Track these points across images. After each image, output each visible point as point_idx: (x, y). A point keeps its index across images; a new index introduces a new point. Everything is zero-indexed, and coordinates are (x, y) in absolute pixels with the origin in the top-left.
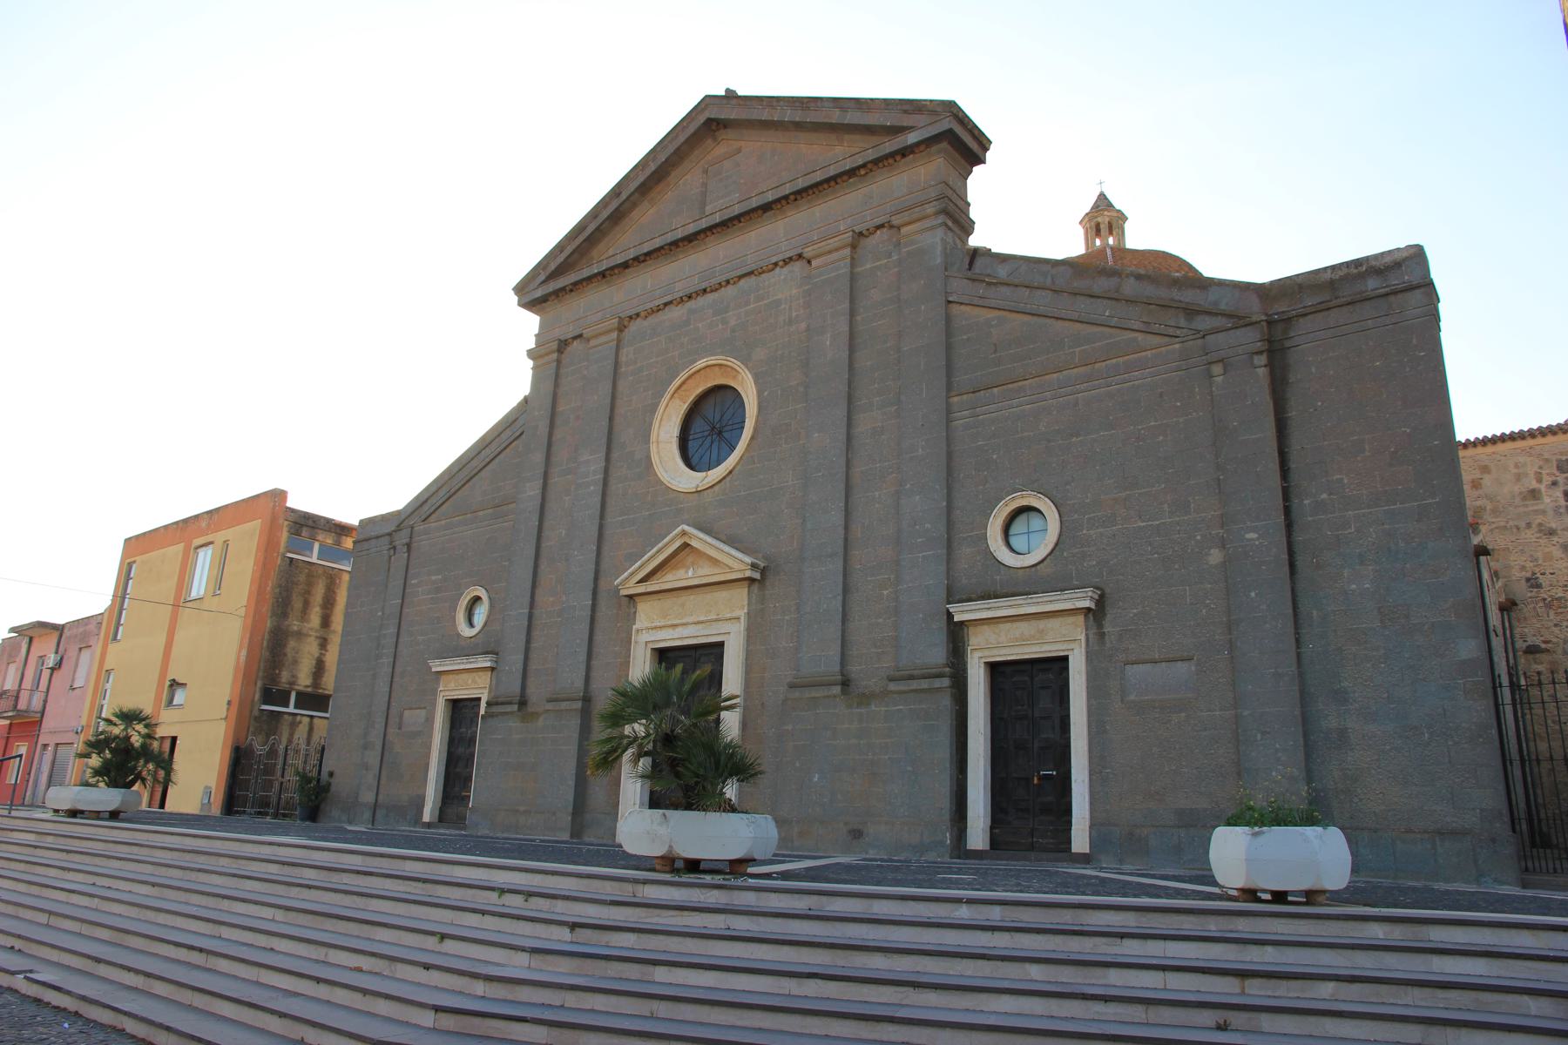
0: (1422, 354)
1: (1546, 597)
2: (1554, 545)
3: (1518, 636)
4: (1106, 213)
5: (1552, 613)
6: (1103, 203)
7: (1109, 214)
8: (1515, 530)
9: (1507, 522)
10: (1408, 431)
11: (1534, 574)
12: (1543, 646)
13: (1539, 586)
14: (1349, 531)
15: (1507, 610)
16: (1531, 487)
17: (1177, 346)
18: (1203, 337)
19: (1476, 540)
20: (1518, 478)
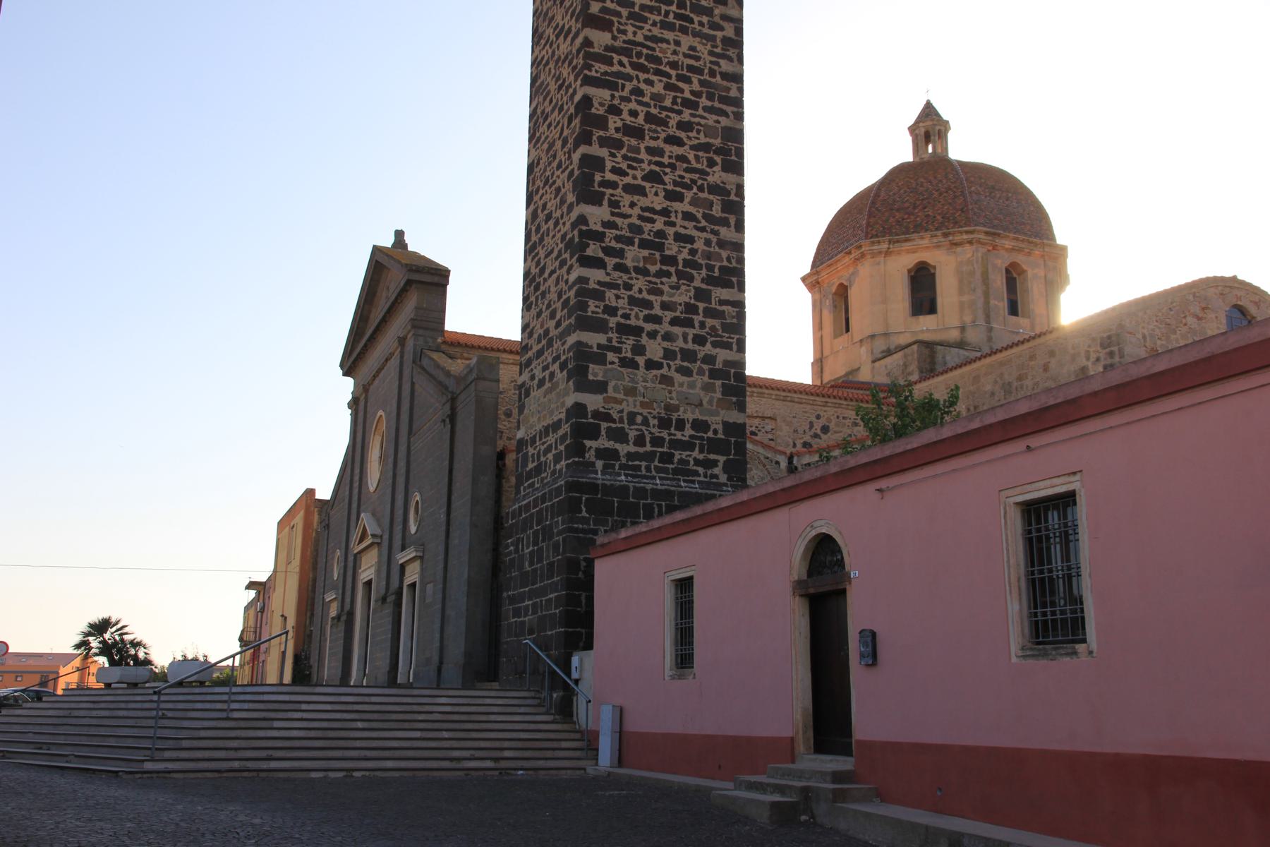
6: (929, 112)
7: (924, 124)
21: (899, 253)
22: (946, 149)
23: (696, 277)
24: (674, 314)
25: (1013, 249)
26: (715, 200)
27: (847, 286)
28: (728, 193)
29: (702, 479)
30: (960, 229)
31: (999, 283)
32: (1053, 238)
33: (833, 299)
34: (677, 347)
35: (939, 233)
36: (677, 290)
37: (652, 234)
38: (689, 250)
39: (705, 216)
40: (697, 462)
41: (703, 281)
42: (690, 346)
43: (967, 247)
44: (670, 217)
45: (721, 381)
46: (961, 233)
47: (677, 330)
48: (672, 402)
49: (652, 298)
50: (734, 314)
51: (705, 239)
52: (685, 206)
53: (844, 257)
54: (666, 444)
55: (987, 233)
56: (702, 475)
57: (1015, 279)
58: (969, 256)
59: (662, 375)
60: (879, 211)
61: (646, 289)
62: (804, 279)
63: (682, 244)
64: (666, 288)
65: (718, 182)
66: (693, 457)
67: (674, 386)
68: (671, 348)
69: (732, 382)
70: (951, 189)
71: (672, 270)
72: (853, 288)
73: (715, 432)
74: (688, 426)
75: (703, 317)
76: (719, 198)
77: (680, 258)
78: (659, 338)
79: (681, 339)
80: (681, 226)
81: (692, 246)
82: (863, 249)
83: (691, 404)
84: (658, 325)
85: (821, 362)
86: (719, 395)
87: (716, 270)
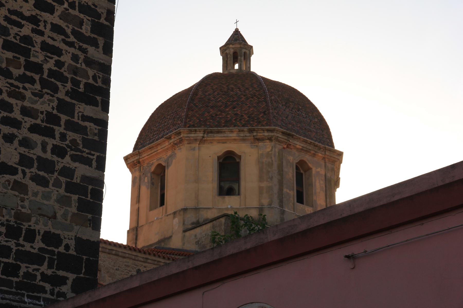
7: (233, 46)
21: (211, 142)
22: (250, 67)
23: (60, 89)
24: (34, 121)
25: (302, 150)
26: (85, 20)
27: (164, 167)
28: (99, 16)
29: (48, 296)
30: (263, 127)
31: (291, 175)
32: (331, 144)
33: (151, 177)
34: (35, 154)
35: (246, 129)
36: (40, 98)
37: (18, 38)
38: (55, 61)
39: (74, 33)
40: (45, 277)
41: (67, 93)
42: (48, 155)
43: (268, 143)
44: (38, 26)
45: (77, 196)
46: (263, 130)
47: (36, 138)
48: (23, 210)
49: (12, 101)
50: (96, 131)
51: (73, 54)
52: (55, 19)
53: (164, 141)
54: (13, 255)
55: (283, 133)
56: (49, 292)
57: (302, 174)
58: (269, 150)
59: (16, 182)
60: (197, 106)
61: (7, 91)
62: (126, 159)
63: (49, 55)
64: (28, 94)
65: (90, 4)
66: (40, 271)
67: (27, 195)
68: (28, 155)
69: (89, 199)
70: (255, 96)
71: (37, 77)
72: (170, 168)
73: (67, 247)
74: (38, 238)
75: (65, 129)
76: (90, 18)
77: (46, 67)
78: (16, 142)
79: (39, 146)
80: (49, 37)
81: (59, 58)
82: (182, 136)
83: (44, 216)
84: (16, 130)
85: (137, 230)
86: (74, 210)
87: (82, 86)
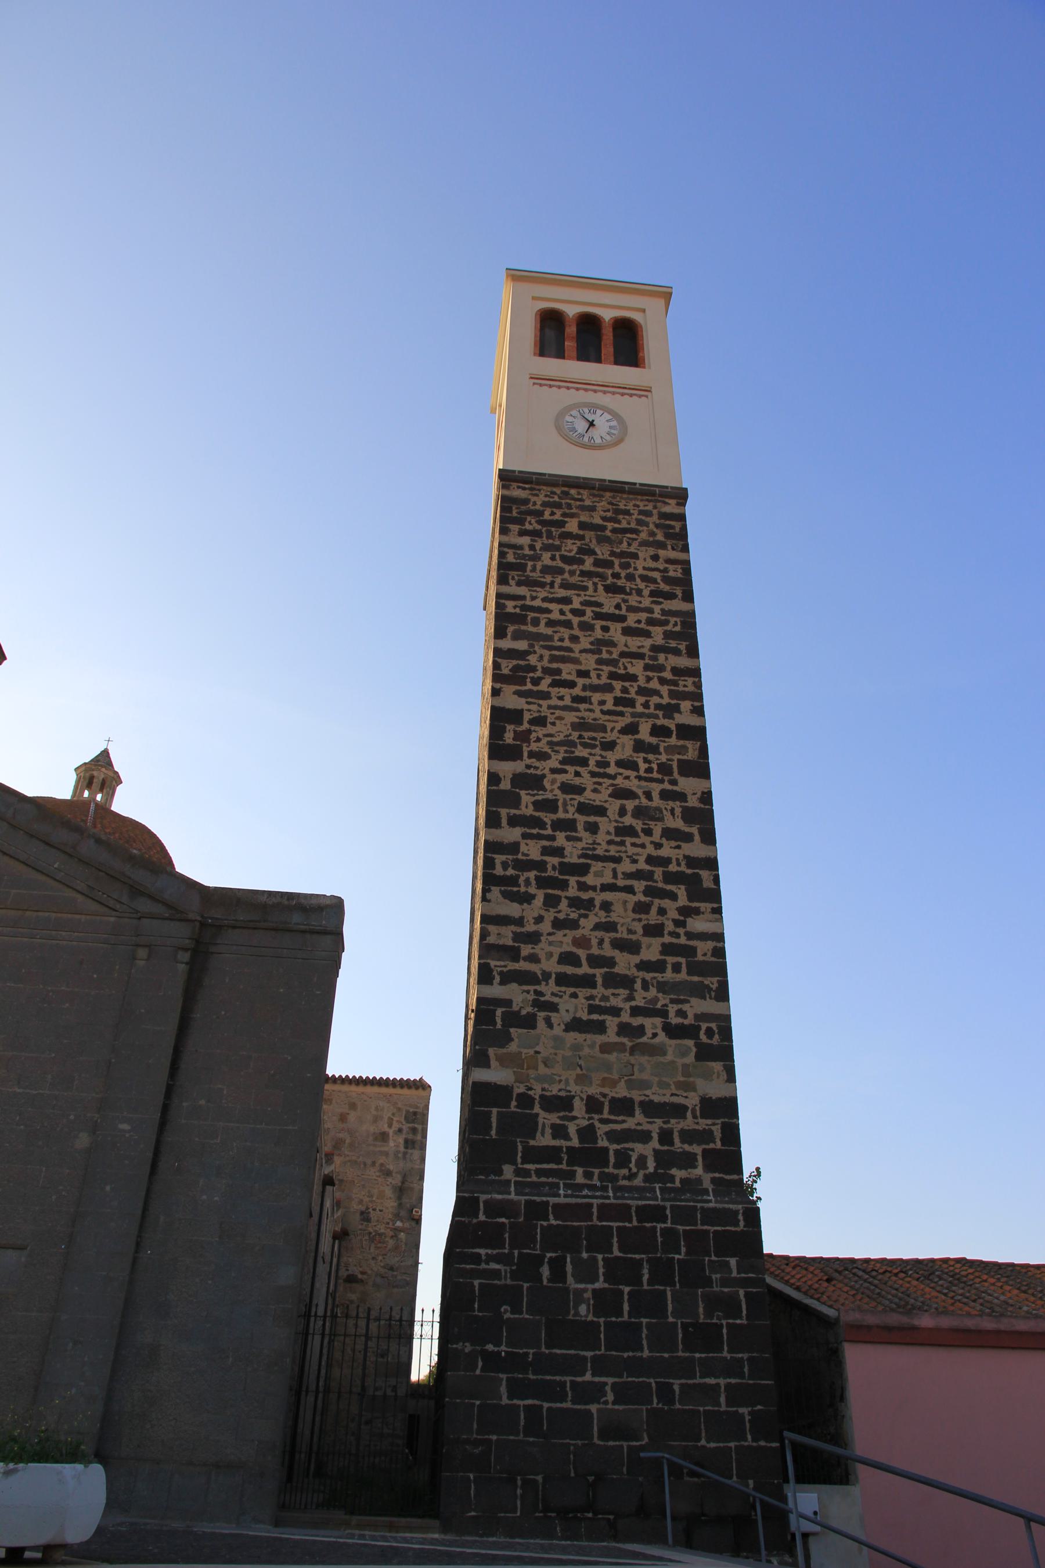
0: (318, 992)
1: (372, 1231)
2: (388, 1185)
3: (342, 1264)
4: (103, 769)
5: (373, 1245)
6: (104, 759)
7: (106, 772)
8: (362, 1166)
9: (359, 1157)
10: (289, 1058)
11: (367, 1208)
12: (360, 1276)
13: (368, 1220)
14: (215, 1141)
15: (338, 1239)
16: (383, 1130)
17: (112, 919)
18: (139, 919)
19: (327, 1170)
20: (376, 1119)
